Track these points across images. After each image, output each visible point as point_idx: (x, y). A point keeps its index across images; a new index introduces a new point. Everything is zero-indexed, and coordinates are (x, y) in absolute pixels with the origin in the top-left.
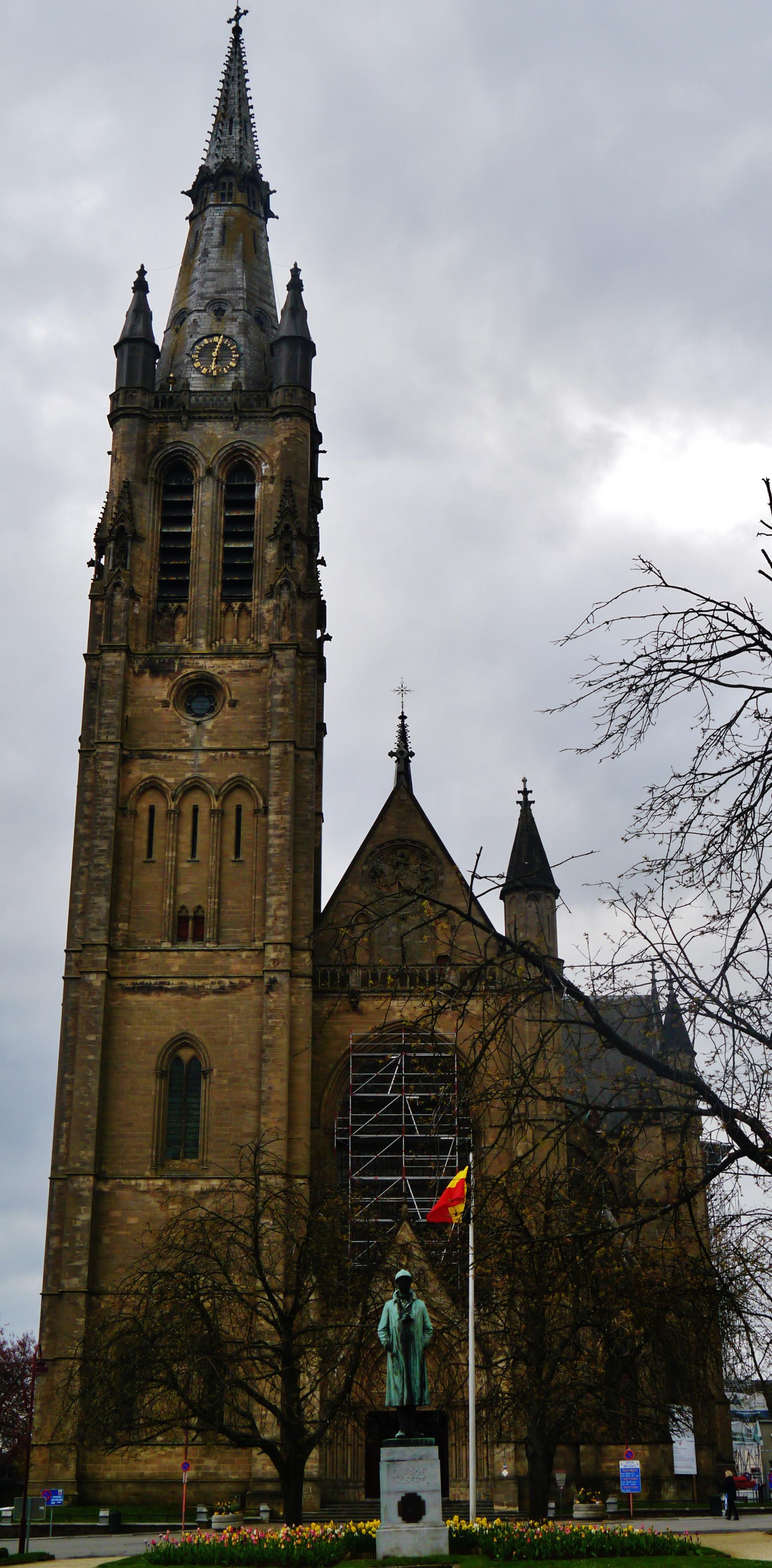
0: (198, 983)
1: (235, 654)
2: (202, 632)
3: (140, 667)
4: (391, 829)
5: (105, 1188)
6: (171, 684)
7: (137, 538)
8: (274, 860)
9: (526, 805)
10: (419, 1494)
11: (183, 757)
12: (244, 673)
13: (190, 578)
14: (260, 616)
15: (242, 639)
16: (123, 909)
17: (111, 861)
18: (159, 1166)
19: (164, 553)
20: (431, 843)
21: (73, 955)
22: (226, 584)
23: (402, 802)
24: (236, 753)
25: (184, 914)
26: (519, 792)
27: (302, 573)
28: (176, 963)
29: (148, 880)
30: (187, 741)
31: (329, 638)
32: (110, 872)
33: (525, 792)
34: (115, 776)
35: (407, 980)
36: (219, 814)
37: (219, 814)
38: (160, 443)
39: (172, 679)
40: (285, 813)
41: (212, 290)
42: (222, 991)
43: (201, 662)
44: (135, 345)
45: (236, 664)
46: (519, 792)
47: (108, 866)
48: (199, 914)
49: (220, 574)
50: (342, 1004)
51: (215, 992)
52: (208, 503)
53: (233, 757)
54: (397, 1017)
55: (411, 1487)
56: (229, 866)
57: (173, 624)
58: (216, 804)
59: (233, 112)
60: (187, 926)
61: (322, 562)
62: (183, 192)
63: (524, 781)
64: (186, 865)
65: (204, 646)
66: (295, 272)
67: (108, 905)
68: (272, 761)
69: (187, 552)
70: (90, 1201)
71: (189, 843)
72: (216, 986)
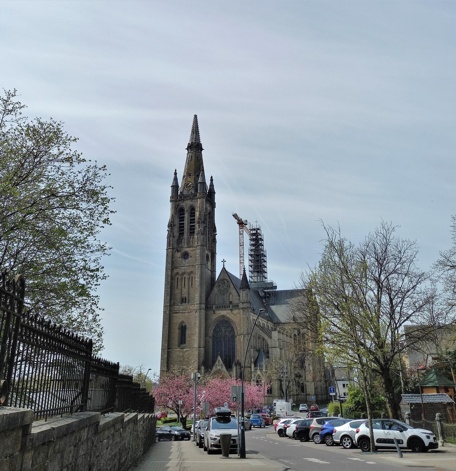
5: (170, 350)
7: (174, 225)
9: (176, 174)
11: (182, 268)
16: (173, 298)
18: (179, 346)
19: (180, 227)
23: (224, 268)
28: (181, 307)
29: (177, 291)
35: (224, 307)
36: (189, 278)
37: (189, 278)
38: (178, 205)
42: (189, 313)
44: (175, 187)
50: (212, 312)
56: (190, 288)
59: (195, 131)
60: (183, 300)
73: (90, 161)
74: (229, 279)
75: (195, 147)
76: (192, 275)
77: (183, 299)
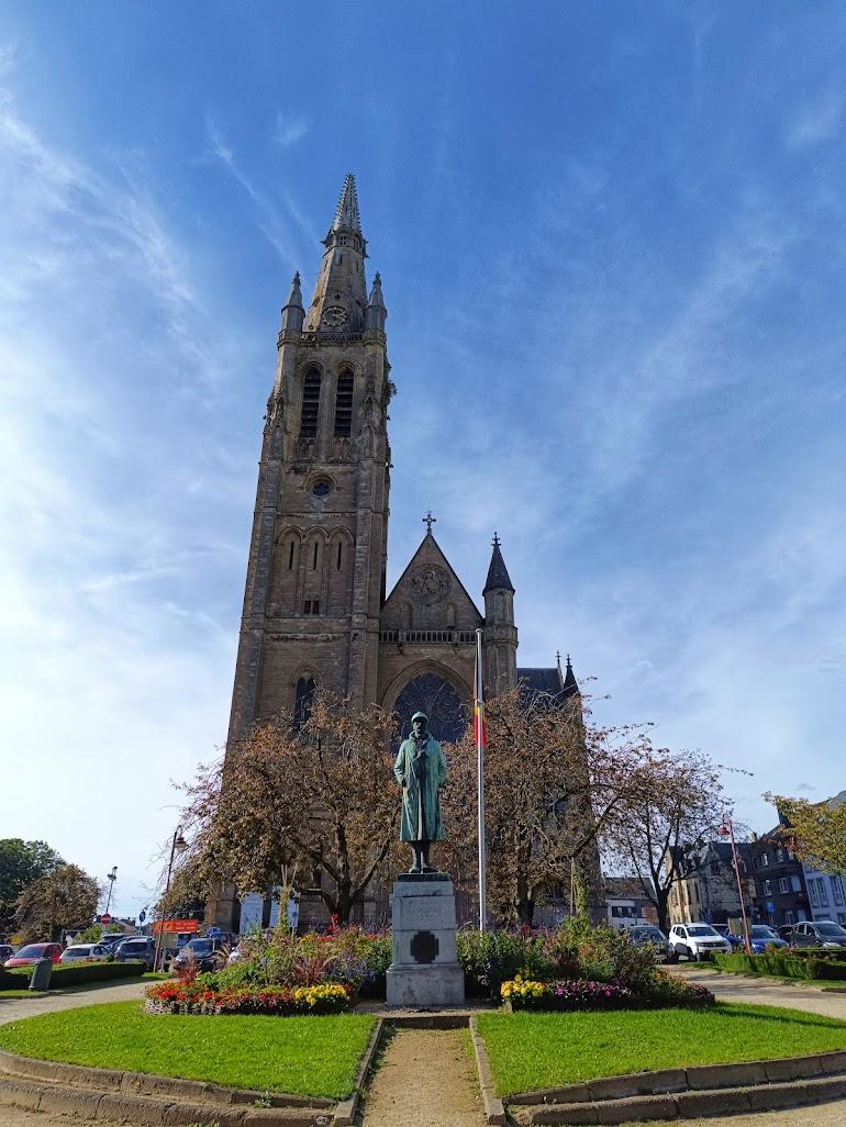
0: (314, 636)
4: (422, 559)
9: (496, 546)
10: (432, 932)
12: (344, 474)
14: (354, 445)
20: (445, 566)
23: (429, 544)
27: (377, 423)
28: (303, 624)
42: (327, 640)
44: (295, 309)
45: (341, 468)
55: (424, 925)
66: (378, 276)
72: (325, 638)
73: (116, 868)
74: (445, 566)
75: (348, 239)
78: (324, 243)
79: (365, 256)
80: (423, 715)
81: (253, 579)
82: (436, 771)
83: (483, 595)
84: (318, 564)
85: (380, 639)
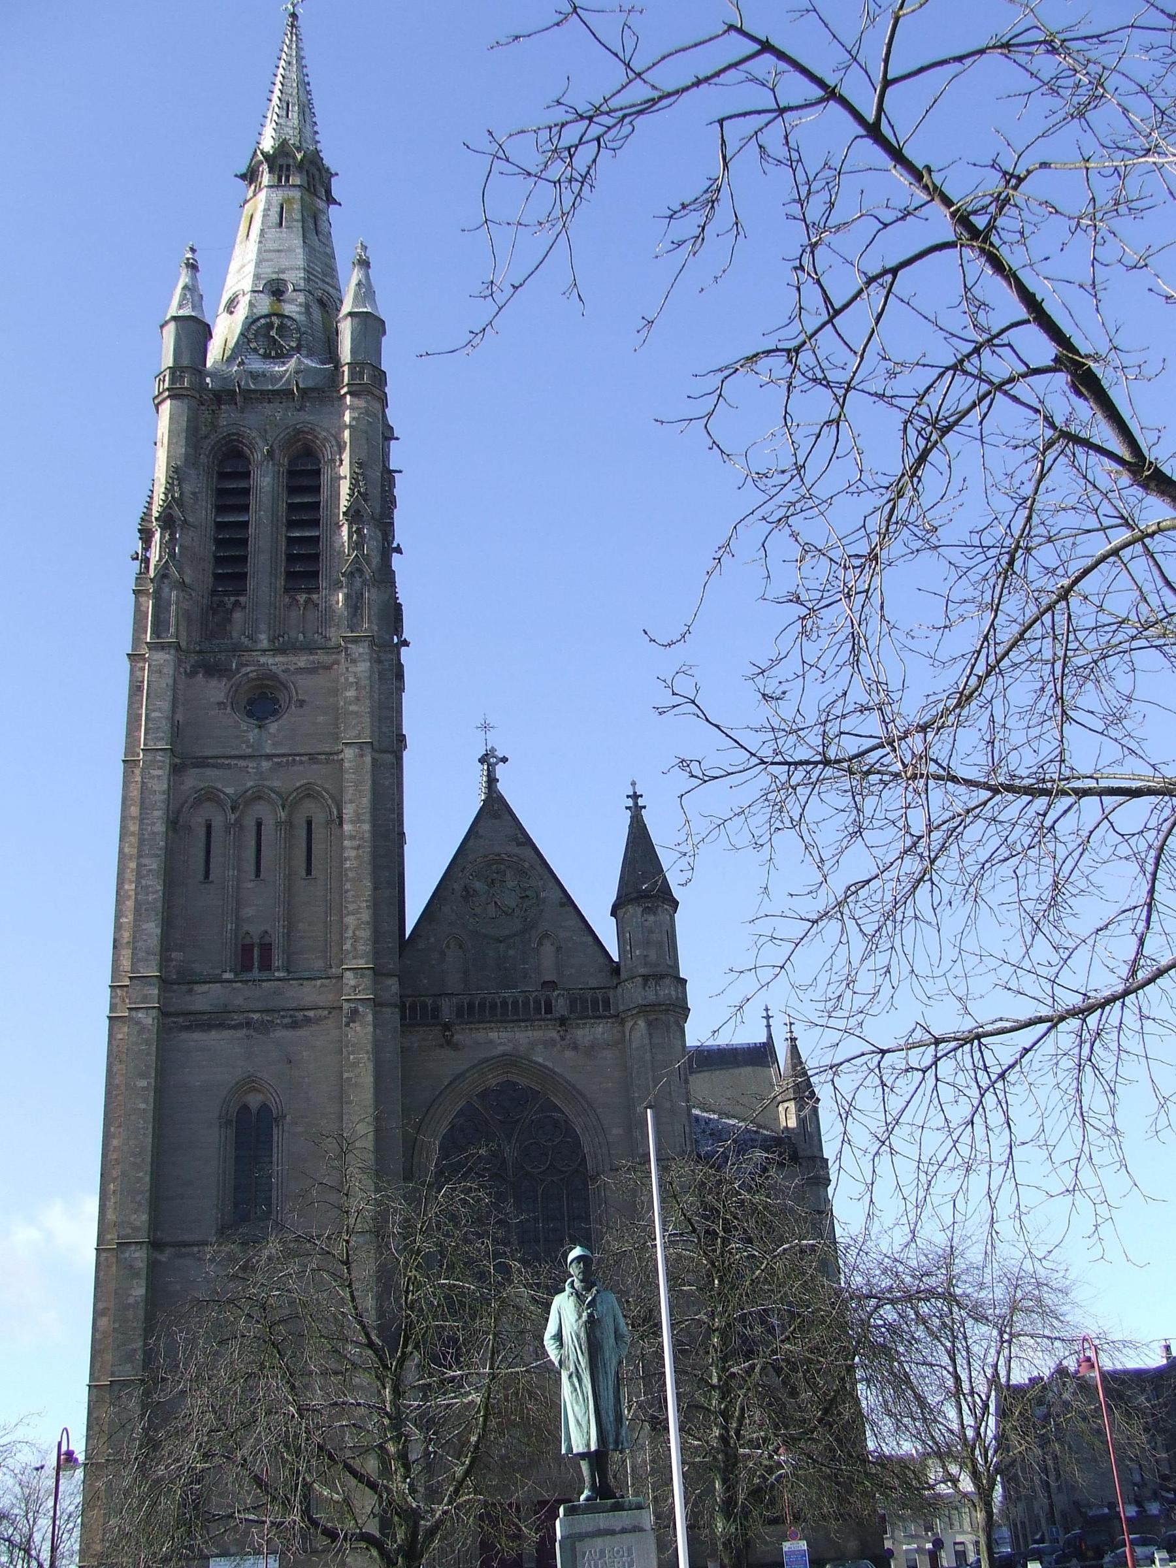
1: (301, 650)
2: (263, 626)
3: (193, 666)
5: (163, 1258)
6: (229, 685)
8: (350, 874)
9: (636, 812)
13: (249, 569)
15: (309, 635)
17: (161, 882)
21: (119, 991)
22: (290, 575)
23: (494, 808)
24: (304, 758)
25: (248, 941)
26: (628, 797)
30: (248, 747)
31: (406, 643)
32: (161, 893)
33: (635, 797)
34: (166, 786)
39: (229, 679)
40: (363, 822)
41: (269, 270)
43: (263, 660)
46: (628, 797)
47: (159, 888)
48: (267, 940)
49: (284, 564)
51: (286, 1027)
52: (268, 489)
53: (301, 762)
54: (500, 1050)
57: (230, 620)
58: (283, 815)
61: (398, 550)
62: (236, 176)
63: (633, 784)
64: (250, 885)
65: (265, 642)
67: (159, 931)
68: (347, 765)
69: (244, 542)
70: (144, 1273)
71: (253, 861)
76: (310, 808)
77: (247, 949)
78: (243, 177)
79: (330, 200)
80: (588, 1253)
81: (130, 903)
82: (612, 1341)
83: (613, 914)
84: (303, 833)
85: (403, 1018)
